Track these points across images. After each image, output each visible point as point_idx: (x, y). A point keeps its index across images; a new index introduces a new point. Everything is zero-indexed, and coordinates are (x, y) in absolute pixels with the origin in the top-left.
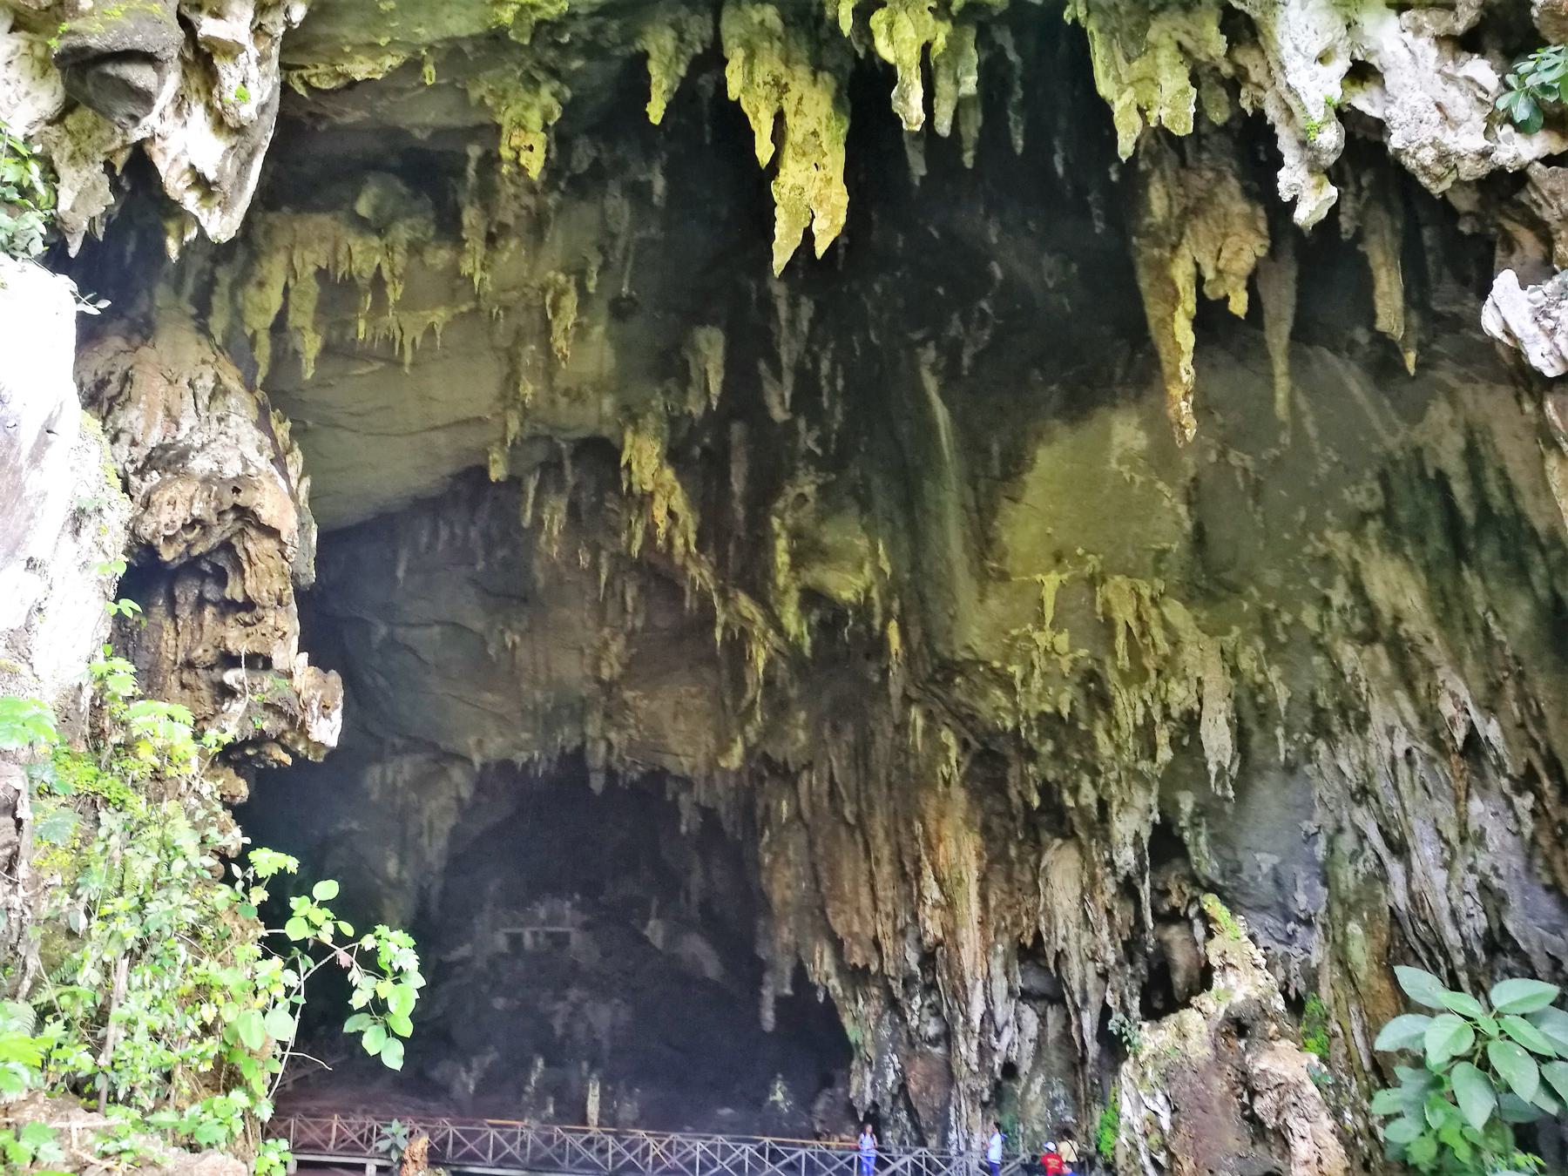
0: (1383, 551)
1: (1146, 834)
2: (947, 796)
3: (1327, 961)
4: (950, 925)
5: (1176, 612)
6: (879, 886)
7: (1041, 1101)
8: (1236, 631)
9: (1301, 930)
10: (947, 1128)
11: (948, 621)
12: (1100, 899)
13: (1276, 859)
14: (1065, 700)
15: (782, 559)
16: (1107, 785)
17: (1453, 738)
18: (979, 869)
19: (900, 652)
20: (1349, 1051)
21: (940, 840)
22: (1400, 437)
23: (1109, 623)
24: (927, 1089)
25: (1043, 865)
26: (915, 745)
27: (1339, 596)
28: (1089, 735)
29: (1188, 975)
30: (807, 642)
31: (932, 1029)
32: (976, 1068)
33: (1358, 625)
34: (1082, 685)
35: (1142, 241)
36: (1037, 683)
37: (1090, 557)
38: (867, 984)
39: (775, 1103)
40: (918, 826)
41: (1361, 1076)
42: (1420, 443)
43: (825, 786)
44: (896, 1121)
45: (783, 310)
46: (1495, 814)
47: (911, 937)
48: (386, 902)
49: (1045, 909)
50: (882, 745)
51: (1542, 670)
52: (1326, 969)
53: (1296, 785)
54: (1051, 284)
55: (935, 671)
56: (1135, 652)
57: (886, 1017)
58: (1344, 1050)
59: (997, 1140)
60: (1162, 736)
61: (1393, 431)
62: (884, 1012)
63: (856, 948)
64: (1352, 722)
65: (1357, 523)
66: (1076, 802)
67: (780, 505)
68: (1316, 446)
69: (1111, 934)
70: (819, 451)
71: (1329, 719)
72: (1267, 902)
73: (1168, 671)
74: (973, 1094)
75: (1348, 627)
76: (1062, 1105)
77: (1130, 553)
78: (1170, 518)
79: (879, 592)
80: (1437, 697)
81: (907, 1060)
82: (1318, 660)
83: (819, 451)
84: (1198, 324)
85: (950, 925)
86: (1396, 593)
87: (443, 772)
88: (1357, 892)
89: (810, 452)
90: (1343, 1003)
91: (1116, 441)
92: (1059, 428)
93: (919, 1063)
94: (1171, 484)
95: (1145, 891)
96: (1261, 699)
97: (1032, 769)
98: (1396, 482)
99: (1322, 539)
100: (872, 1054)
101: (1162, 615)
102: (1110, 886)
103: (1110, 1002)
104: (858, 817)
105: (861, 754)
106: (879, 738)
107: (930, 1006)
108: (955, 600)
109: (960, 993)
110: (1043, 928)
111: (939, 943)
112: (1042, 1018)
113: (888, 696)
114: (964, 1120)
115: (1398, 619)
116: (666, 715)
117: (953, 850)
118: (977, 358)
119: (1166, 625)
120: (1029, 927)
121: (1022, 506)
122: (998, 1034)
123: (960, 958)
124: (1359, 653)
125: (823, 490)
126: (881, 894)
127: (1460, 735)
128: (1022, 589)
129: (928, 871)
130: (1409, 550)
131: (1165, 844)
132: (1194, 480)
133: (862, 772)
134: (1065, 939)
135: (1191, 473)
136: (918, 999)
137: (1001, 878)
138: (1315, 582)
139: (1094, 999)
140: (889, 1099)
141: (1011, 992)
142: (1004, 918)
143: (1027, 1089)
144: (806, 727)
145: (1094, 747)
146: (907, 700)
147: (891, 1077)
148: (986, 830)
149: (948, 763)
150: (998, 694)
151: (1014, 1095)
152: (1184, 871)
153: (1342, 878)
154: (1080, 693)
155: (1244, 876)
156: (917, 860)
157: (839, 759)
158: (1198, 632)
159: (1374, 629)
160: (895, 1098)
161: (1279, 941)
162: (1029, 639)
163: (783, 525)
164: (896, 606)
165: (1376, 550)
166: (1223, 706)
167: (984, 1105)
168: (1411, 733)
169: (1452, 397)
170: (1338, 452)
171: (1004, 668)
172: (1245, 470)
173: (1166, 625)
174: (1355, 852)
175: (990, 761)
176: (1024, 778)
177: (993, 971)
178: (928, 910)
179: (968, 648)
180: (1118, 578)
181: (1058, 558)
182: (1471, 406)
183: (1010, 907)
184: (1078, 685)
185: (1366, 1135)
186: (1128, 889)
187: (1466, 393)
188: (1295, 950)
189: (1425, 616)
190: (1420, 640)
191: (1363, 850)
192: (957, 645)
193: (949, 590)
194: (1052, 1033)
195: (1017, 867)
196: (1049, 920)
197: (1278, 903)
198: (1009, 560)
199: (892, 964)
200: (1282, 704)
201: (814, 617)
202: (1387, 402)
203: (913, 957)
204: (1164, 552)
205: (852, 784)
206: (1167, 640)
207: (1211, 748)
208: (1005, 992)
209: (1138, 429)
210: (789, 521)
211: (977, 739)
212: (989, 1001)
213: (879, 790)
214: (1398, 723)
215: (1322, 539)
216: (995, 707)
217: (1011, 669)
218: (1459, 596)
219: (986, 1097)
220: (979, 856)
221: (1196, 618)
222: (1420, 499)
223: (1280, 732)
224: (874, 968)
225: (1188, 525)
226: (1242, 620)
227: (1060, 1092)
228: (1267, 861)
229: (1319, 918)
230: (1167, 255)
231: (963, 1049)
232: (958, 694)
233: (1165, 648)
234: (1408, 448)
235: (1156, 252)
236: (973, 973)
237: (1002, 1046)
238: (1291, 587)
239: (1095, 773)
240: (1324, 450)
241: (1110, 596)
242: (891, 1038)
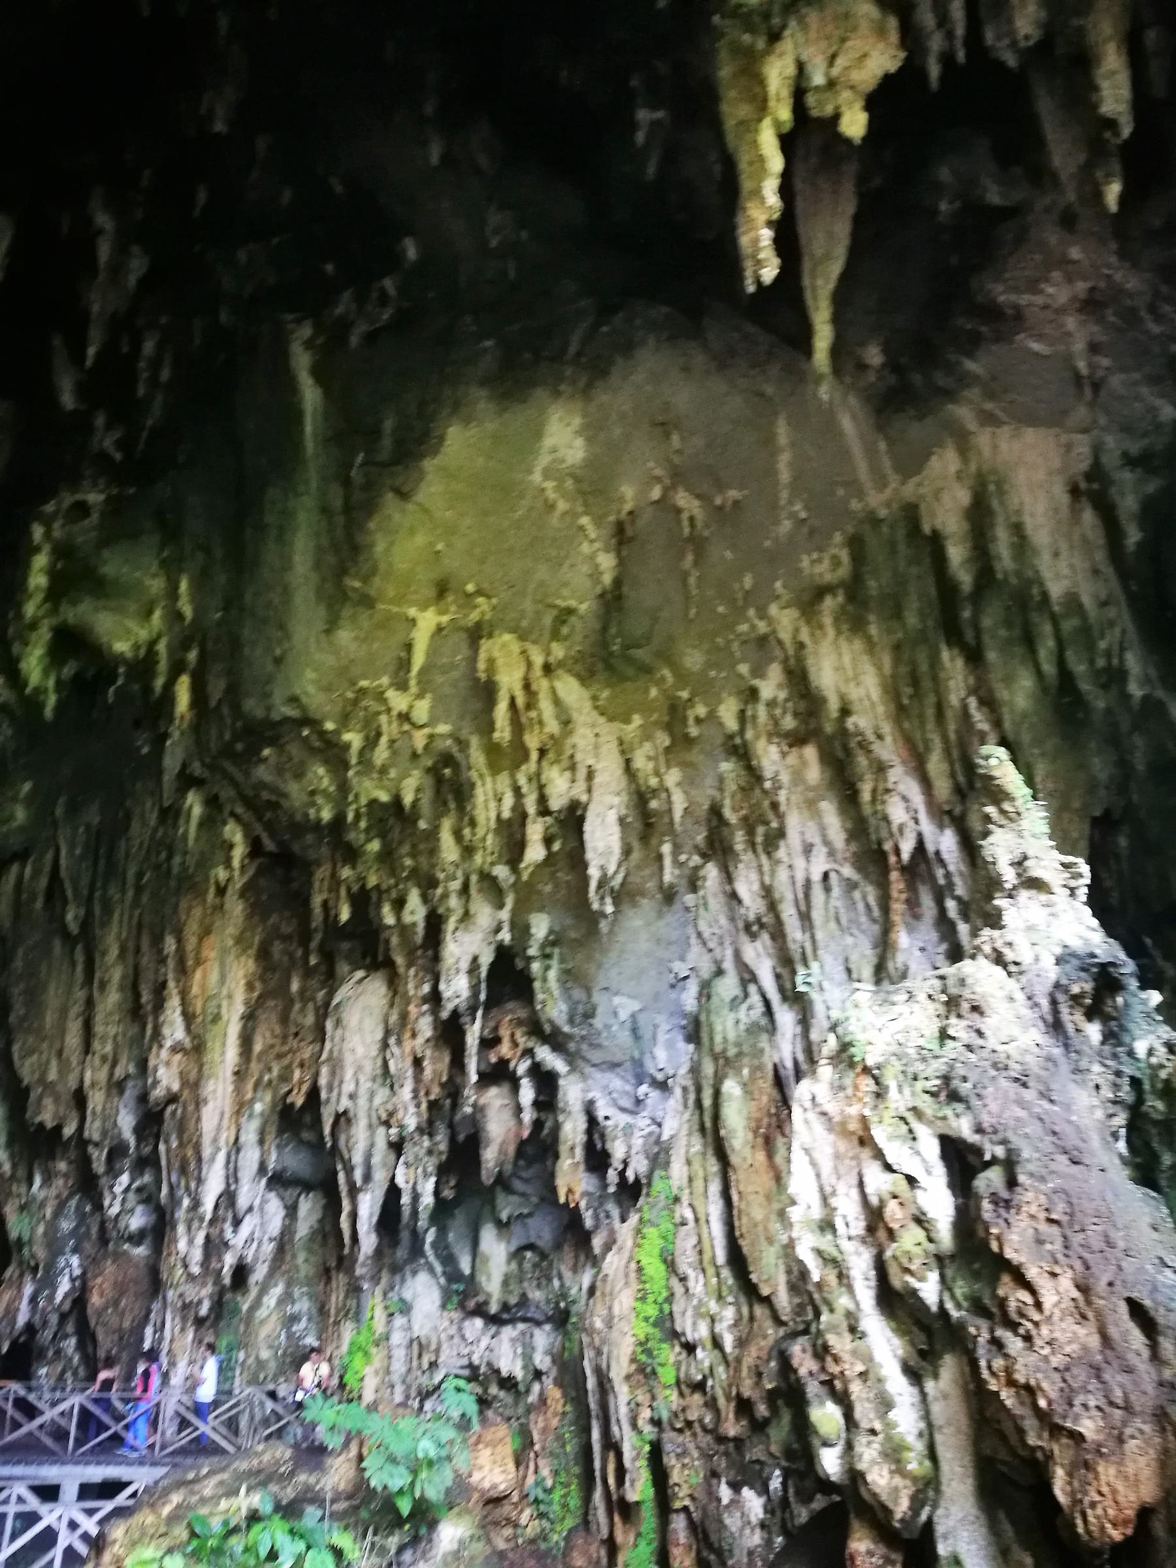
0: (839, 632)
1: (486, 959)
2: (220, 908)
3: (684, 1132)
4: (193, 1076)
5: (570, 689)
6: (99, 1018)
7: (274, 1317)
8: (637, 720)
9: (655, 1094)
11: (270, 667)
12: (408, 1045)
13: (635, 1006)
14: (412, 786)
15: (38, 580)
16: (445, 896)
17: (897, 851)
18: (247, 1003)
19: (188, 717)
20: (700, 1242)
21: (199, 962)
22: (888, 492)
23: (487, 691)
24: (116, 1303)
25: (335, 1002)
26: (185, 837)
27: (771, 686)
28: (433, 835)
29: (502, 1151)
30: (52, 700)
31: (137, 1221)
33: (789, 723)
34: (434, 772)
35: (728, 22)
36: (381, 754)
37: (480, 600)
38: (52, 1157)
40: (170, 945)
41: (711, 1271)
42: (913, 499)
43: (43, 882)
44: (58, 1352)
45: (104, 251)
46: (922, 949)
47: (130, 1093)
49: (330, 1059)
50: (143, 827)
51: (1043, 754)
52: (682, 1141)
53: (673, 917)
54: (494, 243)
55: (236, 737)
56: (518, 727)
57: (73, 1203)
58: (693, 1240)
59: (210, 1369)
60: (535, 831)
61: (881, 483)
62: (70, 1196)
64: (759, 839)
65: (809, 601)
66: (399, 919)
67: (50, 508)
68: (784, 495)
69: (415, 1092)
70: (118, 456)
71: (732, 834)
72: (618, 1057)
73: (551, 755)
74: (186, 1307)
75: (776, 723)
76: (303, 1323)
77: (528, 605)
78: (585, 569)
79: (169, 647)
80: (884, 802)
81: (91, 1265)
82: (727, 767)
83: (118, 456)
84: (787, 143)
86: (847, 681)
88: (738, 1044)
89: (104, 456)
90: (699, 1184)
91: (548, 442)
92: (481, 400)
93: (109, 1267)
94: (598, 521)
95: (473, 1034)
96: (654, 804)
97: (346, 873)
98: (873, 545)
99: (763, 614)
100: (41, 1253)
101: (553, 691)
102: (426, 1027)
103: (400, 1181)
104: (86, 924)
105: (104, 847)
106: (135, 826)
107: (139, 1190)
108: (288, 636)
109: (190, 1167)
110: (323, 1081)
111: (173, 1098)
112: (291, 1211)
113: (160, 772)
115: (845, 712)
117: (214, 977)
118: (371, 338)
119: (557, 701)
120: (301, 1082)
121: (410, 507)
122: (237, 1223)
123: (199, 1119)
124: (784, 755)
125: (115, 507)
126: (99, 1029)
127: (907, 847)
128: (385, 624)
129: (173, 1006)
130: (873, 630)
131: (507, 978)
132: (631, 513)
133: (102, 862)
134: (352, 1097)
135: (628, 507)
136: (125, 1179)
137: (274, 1018)
138: (743, 669)
139: (380, 1177)
140: (54, 1319)
141: (262, 1169)
142: (270, 1070)
143: (257, 1304)
144: (29, 801)
145: (434, 851)
146: (187, 781)
147: (64, 1286)
148: (263, 955)
149: (228, 863)
150: (320, 775)
151: (236, 1310)
152: (522, 1013)
153: (718, 1028)
154: (429, 782)
155: (598, 1022)
156: (160, 989)
157: (72, 847)
158: (595, 713)
159: (814, 723)
160: (63, 1317)
161: (623, 1110)
162: (380, 697)
163: (48, 535)
164: (192, 656)
165: (831, 632)
166: (616, 800)
167: (199, 1322)
168: (832, 853)
169: (964, 446)
170: (807, 508)
171: (337, 732)
172: (692, 519)
173: (557, 701)
174: (735, 999)
175: (283, 869)
176: (335, 882)
177: (242, 1139)
178: (164, 1054)
179: (294, 700)
180: (507, 637)
181: (442, 589)
182: (987, 451)
183: (280, 1056)
184: (429, 770)
185: (709, 1345)
186: (450, 1033)
187: (983, 439)
188: (642, 1122)
189: (881, 709)
190: (872, 737)
191: (746, 995)
192: (278, 697)
193: (282, 627)
194: (303, 1229)
195: (297, 1006)
196: (333, 1073)
197: (633, 1059)
198: (377, 581)
199: (97, 1124)
200: (678, 814)
201: (68, 671)
202: (882, 446)
203: (126, 1122)
204: (570, 611)
205: (85, 882)
206: (557, 717)
207: (595, 849)
208: (255, 1166)
209: (578, 433)
210: (57, 533)
211: (272, 836)
212: (232, 1176)
213: (123, 891)
214: (817, 840)
215: (763, 614)
216: (312, 791)
217: (347, 737)
218: (935, 679)
219: (204, 1310)
220: (250, 986)
221: (595, 698)
222: (902, 565)
223: (666, 849)
224: (69, 1131)
225: (607, 579)
226: (646, 708)
227: (303, 1305)
228: (626, 1006)
229: (679, 1079)
230: (761, 44)
231: (182, 1245)
232: (262, 773)
233: (553, 726)
234: (895, 506)
235: (747, 38)
236: (215, 1140)
237: (237, 1240)
238: (713, 673)
239: (428, 884)
240: (790, 502)
241: (496, 654)
242: (74, 1233)
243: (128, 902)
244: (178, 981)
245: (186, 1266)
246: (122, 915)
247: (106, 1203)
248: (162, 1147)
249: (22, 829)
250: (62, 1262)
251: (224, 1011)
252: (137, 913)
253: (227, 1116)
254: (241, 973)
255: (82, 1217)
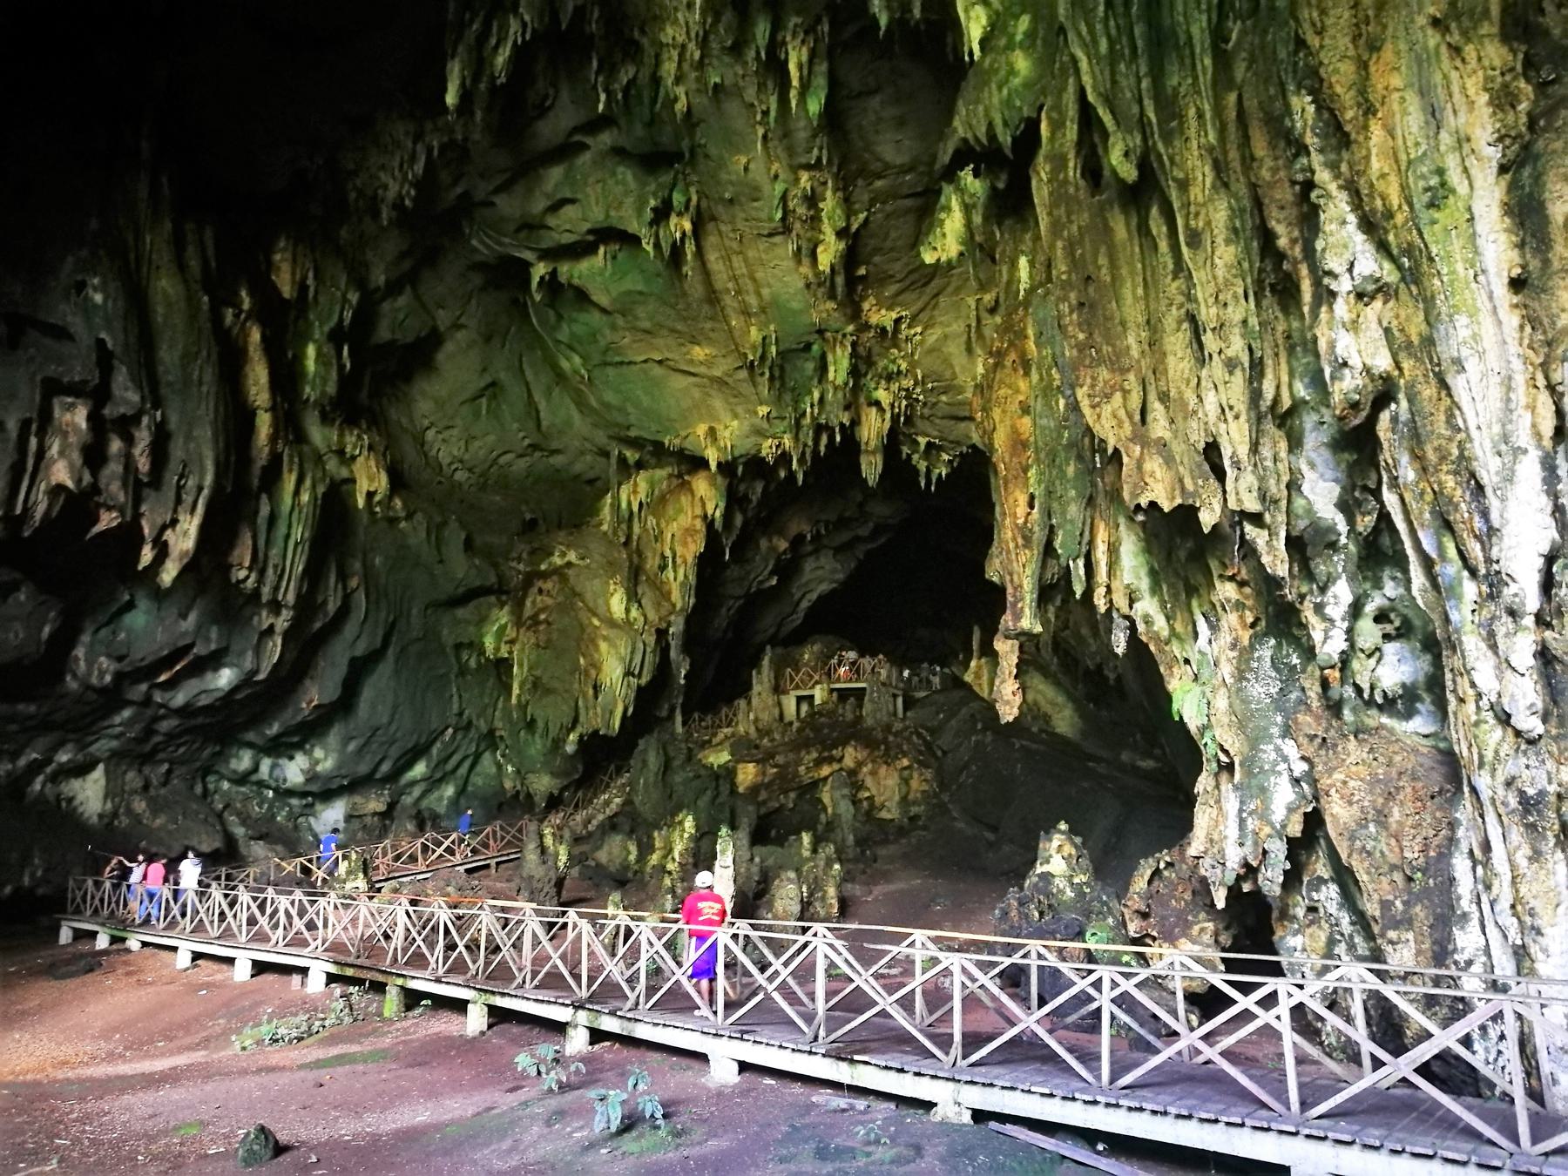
10: (1446, 918)
24: (1381, 817)
31: (1395, 669)
32: (1534, 726)
39: (1047, 877)
40: (1303, 108)
48: (603, 646)
57: (1266, 652)
62: (1257, 639)
63: (1154, 465)
85: (1416, 328)
87: (685, 486)
100: (1235, 744)
107: (1381, 617)
111: (1384, 395)
114: (1503, 890)
116: (955, 349)
117: (1412, 121)
136: (1342, 593)
140: (1278, 849)
147: (1283, 796)
220: (1503, 99)
242: (1279, 702)
243: (1205, 80)
244: (1333, 167)
245: (1505, 719)
246: (1200, 115)
247: (1317, 636)
248: (1390, 498)
249: (1027, 85)
250: (1268, 753)
251: (1455, 178)
252: (1232, 98)
253: (1520, 380)
254: (1473, 85)
255: (1289, 676)
